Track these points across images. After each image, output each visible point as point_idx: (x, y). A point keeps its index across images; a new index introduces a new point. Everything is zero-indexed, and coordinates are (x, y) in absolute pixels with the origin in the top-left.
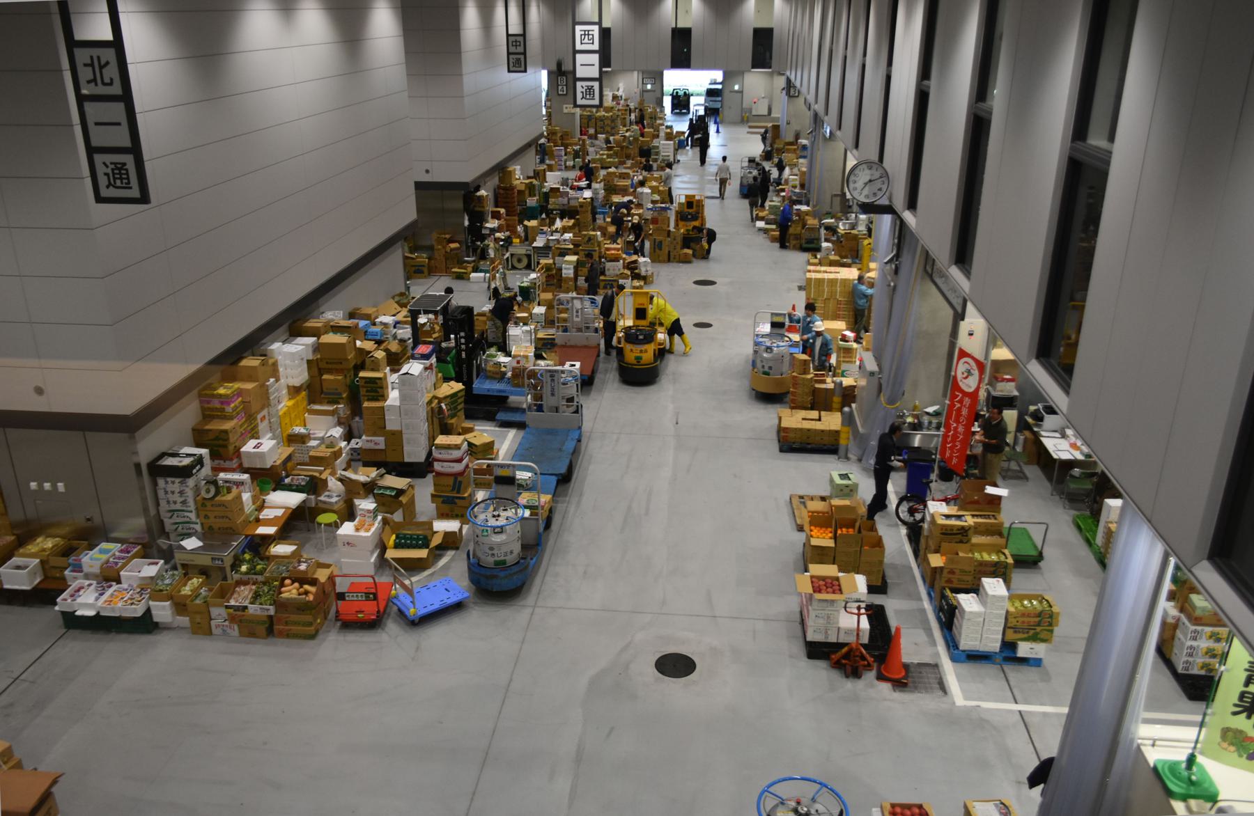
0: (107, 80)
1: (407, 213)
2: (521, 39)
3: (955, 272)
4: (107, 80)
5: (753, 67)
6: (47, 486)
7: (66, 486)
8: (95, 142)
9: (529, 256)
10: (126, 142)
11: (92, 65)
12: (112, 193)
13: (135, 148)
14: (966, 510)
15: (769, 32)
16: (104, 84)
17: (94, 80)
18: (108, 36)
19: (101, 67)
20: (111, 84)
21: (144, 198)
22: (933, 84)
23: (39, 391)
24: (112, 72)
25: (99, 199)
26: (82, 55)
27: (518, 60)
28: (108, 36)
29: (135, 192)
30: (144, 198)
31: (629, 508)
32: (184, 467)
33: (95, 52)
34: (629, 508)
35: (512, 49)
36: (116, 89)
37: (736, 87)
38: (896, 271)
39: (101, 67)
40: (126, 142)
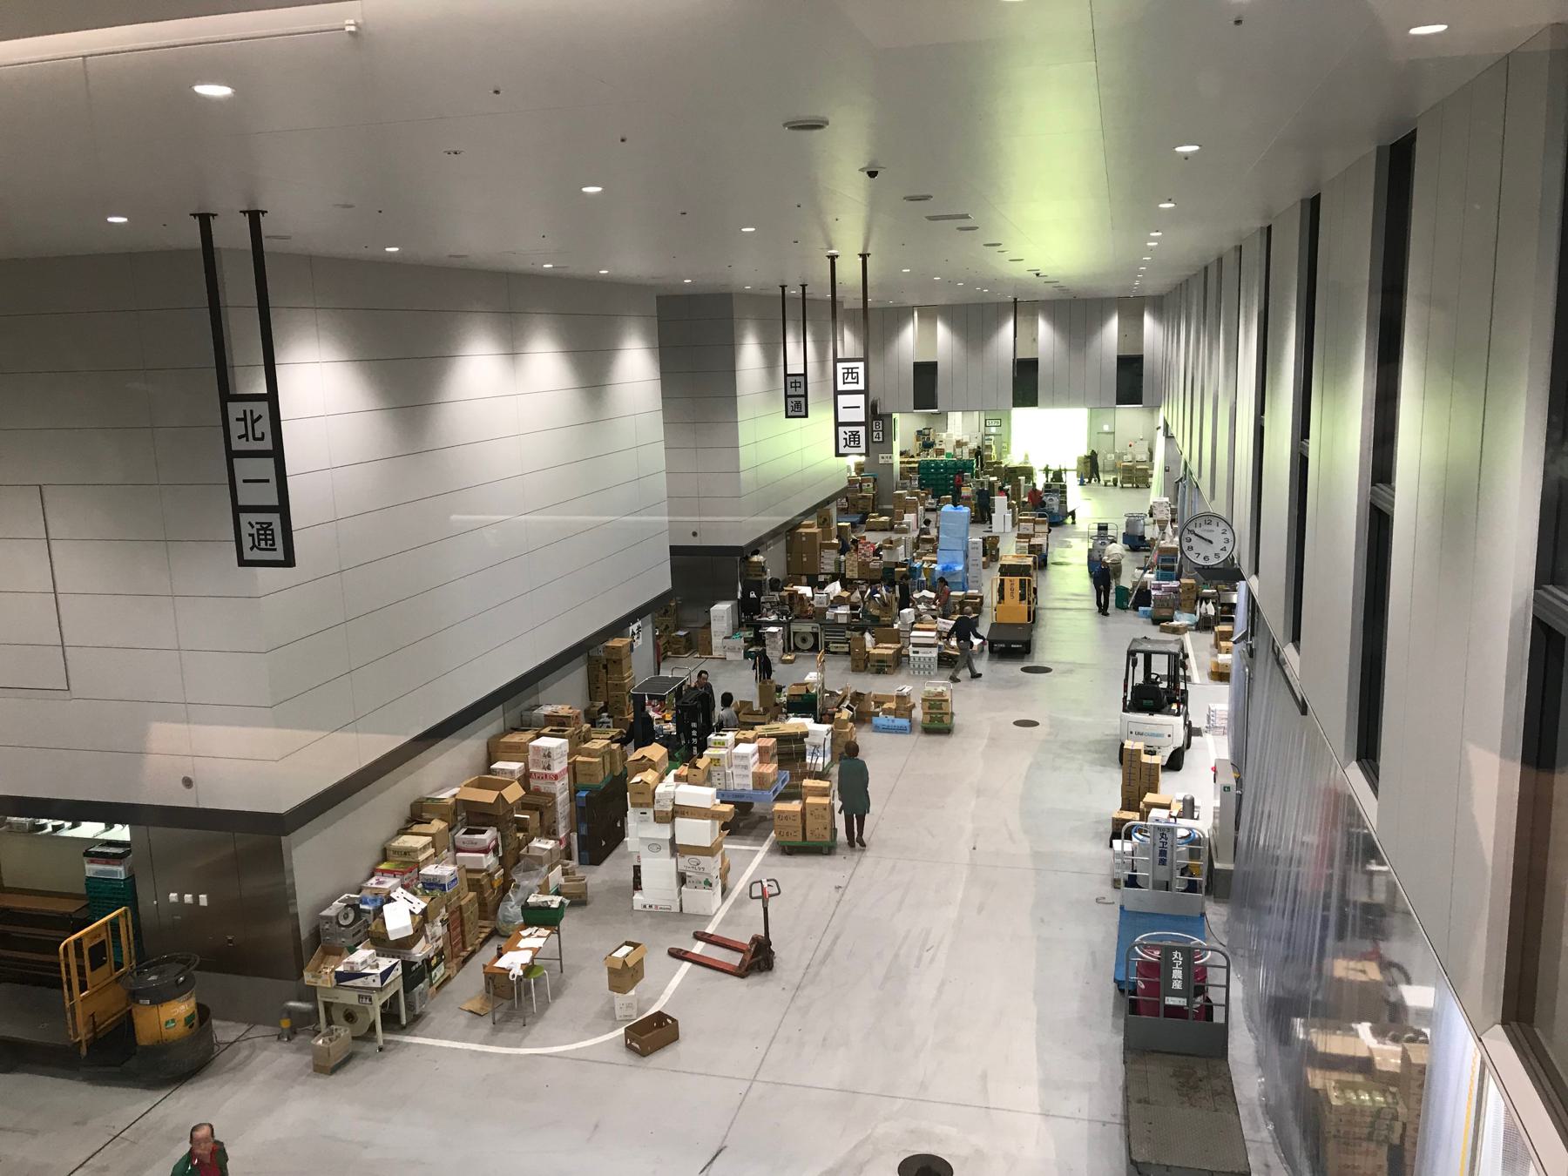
0: (258, 435)
1: (662, 582)
2: (802, 379)
3: (1289, 652)
4: (258, 435)
5: (1119, 402)
6: (188, 898)
7: (209, 899)
8: (243, 501)
9: (815, 635)
10: (274, 501)
11: (245, 419)
12: (257, 555)
13: (283, 508)
14: (574, 826)
15: (1033, 364)
16: (255, 439)
17: (246, 435)
18: (264, 390)
19: (253, 422)
20: (262, 439)
21: (289, 561)
22: (1266, 417)
23: (188, 783)
24: (264, 426)
25: (243, 562)
26: (235, 409)
27: (798, 403)
28: (264, 390)
29: (279, 555)
30: (289, 561)
31: (896, 956)
32: (532, 925)
33: (248, 406)
34: (896, 956)
35: (791, 391)
36: (267, 444)
37: (1106, 428)
38: (1251, 653)
39: (253, 422)
40: (274, 501)
